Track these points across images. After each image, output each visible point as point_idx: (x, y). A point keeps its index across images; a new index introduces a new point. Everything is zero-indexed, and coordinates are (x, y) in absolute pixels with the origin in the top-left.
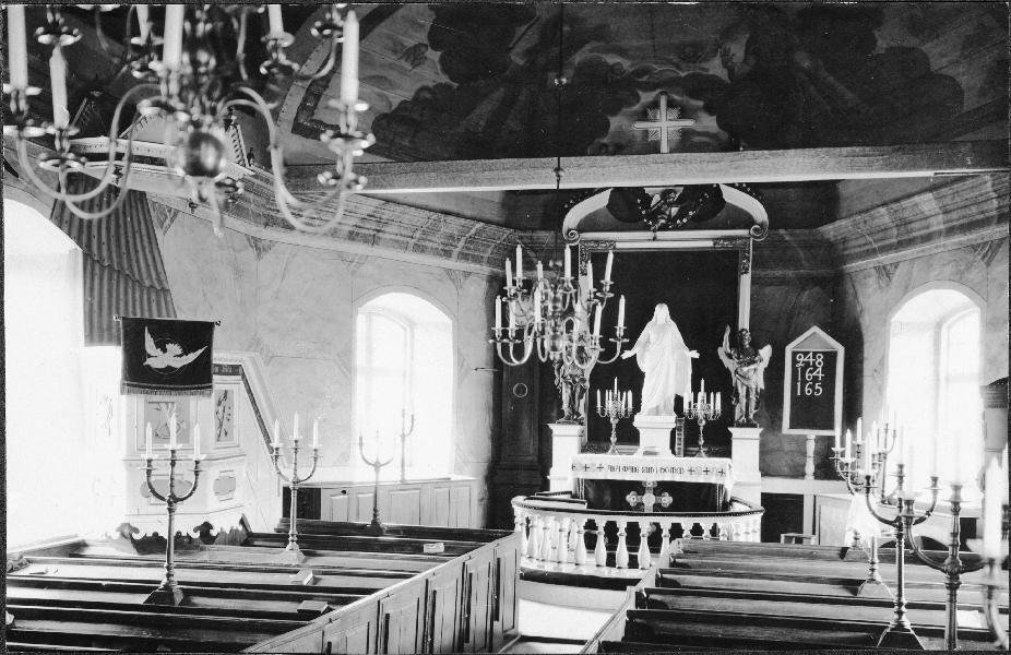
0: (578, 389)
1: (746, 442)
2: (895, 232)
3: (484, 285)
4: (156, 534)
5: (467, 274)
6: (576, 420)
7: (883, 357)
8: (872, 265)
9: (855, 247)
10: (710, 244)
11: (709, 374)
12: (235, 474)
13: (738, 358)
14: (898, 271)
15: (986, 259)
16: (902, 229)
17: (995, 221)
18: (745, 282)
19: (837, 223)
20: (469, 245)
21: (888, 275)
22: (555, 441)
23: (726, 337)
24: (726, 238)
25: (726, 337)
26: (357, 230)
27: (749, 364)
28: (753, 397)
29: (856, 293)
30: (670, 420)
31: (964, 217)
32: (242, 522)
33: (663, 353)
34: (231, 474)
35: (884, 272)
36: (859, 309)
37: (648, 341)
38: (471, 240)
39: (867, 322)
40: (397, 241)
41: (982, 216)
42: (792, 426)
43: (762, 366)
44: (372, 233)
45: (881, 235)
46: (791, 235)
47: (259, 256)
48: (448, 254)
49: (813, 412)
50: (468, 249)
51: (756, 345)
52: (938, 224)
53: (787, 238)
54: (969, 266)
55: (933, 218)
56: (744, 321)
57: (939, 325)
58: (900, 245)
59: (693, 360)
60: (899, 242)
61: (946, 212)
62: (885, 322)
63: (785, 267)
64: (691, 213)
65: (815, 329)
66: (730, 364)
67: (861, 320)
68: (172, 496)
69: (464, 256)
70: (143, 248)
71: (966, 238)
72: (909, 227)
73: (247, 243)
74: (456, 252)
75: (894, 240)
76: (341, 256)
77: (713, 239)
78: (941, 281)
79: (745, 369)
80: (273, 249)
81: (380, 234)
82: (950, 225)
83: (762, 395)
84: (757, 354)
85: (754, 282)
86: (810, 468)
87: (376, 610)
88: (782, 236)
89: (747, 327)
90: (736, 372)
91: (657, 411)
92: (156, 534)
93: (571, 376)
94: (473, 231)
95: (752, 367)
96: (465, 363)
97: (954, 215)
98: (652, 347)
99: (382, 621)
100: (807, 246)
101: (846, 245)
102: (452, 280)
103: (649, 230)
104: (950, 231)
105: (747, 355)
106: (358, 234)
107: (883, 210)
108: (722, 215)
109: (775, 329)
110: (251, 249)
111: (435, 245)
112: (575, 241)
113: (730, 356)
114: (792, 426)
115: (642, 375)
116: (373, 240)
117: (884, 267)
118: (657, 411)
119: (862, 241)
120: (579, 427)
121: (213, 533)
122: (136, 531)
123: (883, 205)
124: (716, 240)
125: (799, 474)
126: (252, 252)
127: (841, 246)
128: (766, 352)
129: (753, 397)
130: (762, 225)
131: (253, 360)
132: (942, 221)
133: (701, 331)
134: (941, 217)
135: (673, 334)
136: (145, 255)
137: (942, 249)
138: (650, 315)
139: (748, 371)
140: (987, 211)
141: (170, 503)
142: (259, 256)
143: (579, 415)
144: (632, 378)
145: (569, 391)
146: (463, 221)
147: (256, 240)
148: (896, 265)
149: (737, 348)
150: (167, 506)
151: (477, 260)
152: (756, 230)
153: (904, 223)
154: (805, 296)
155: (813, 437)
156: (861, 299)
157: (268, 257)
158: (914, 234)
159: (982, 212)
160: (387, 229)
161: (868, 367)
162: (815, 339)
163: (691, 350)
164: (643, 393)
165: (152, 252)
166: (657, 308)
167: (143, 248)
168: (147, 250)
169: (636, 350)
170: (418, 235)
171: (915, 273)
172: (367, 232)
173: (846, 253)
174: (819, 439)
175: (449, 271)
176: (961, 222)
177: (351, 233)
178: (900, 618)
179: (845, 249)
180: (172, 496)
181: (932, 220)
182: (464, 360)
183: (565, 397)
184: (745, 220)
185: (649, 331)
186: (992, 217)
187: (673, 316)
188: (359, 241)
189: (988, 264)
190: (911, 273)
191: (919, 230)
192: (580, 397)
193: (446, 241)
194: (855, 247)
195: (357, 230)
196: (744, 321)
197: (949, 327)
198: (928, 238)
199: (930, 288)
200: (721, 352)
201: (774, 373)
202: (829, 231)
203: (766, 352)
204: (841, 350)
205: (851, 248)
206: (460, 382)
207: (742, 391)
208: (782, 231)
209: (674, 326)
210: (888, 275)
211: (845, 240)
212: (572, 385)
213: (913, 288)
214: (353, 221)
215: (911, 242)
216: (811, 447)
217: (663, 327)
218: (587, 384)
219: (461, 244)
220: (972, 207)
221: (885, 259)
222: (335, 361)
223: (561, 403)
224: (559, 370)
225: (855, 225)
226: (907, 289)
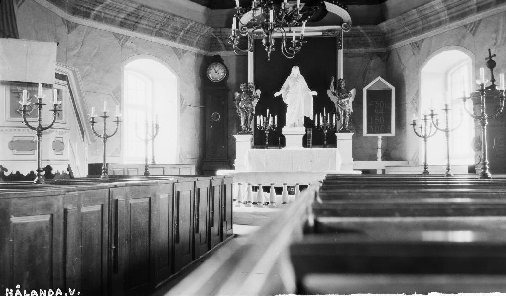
0: (250, 115)
1: (345, 140)
2: (421, 22)
3: (194, 57)
4: (18, 172)
5: (185, 51)
6: (249, 132)
7: (418, 91)
8: (408, 43)
9: (399, 34)
10: (320, 33)
11: (321, 104)
12: (64, 140)
13: (339, 95)
14: (423, 44)
15: (473, 32)
16: (425, 21)
17: (476, 11)
18: (341, 54)
19: (388, 21)
20: (186, 35)
21: (418, 47)
22: (237, 144)
23: (332, 84)
24: (329, 31)
25: (332, 84)
26: (125, 21)
27: (345, 98)
28: (347, 116)
29: (400, 59)
30: (303, 130)
31: (459, 11)
32: (68, 169)
33: (297, 94)
34: (61, 140)
35: (417, 46)
36: (402, 67)
37: (288, 87)
38: (188, 31)
39: (408, 74)
40: (146, 29)
41: (468, 9)
42: (368, 132)
43: (351, 100)
44: (133, 23)
45: (413, 25)
46: (363, 29)
47: (69, 32)
48: (174, 39)
49: (379, 123)
50: (185, 37)
51: (348, 89)
52: (445, 16)
53: (362, 31)
54: (464, 37)
55: (442, 13)
56: (341, 75)
57: (446, 74)
58: (423, 31)
59: (314, 96)
60: (423, 28)
61: (448, 9)
62: (417, 72)
63: (360, 47)
64: (309, 17)
65: (379, 78)
66: (334, 99)
67: (404, 73)
68: (40, 126)
69: (183, 41)
70: (7, 13)
71: (461, 21)
72: (428, 19)
73: (62, 23)
74: (178, 39)
75: (420, 28)
76: (116, 35)
77: (322, 31)
78: (449, 46)
79: (343, 100)
80: (77, 28)
81: (137, 24)
82: (451, 16)
83: (352, 115)
84: (349, 92)
85: (345, 55)
86: (379, 154)
87: (172, 188)
88: (359, 30)
89: (342, 78)
90: (338, 103)
91: (294, 125)
92: (18, 172)
93: (245, 107)
94: (188, 27)
95: (347, 99)
96: (184, 102)
97: (453, 10)
98: (290, 90)
99: (176, 195)
100: (371, 34)
101: (393, 34)
102: (177, 54)
103: (287, 26)
104: (452, 19)
105: (342, 93)
106: (125, 23)
107: (414, 11)
108: (326, 18)
109: (356, 80)
110: (64, 26)
111: (167, 33)
112: (246, 32)
113: (334, 94)
114: (368, 132)
115: (285, 106)
116: (133, 28)
117: (416, 43)
118: (294, 125)
119: (402, 30)
120: (251, 135)
121: (53, 172)
122: (7, 170)
123: (414, 9)
124: (323, 31)
125: (373, 158)
126: (64, 29)
127: (391, 34)
128: (353, 92)
129: (347, 116)
130: (348, 23)
131: (74, 73)
132: (446, 14)
133: (318, 80)
134: (446, 12)
135: (302, 83)
136: (7, 16)
137: (448, 29)
138: (288, 73)
139: (345, 101)
140: (471, 6)
141: (38, 131)
142: (69, 32)
143: (250, 129)
144: (280, 109)
145: (245, 116)
146: (183, 20)
147: (68, 22)
148: (423, 41)
149: (338, 89)
150: (36, 133)
151: (190, 44)
152: (345, 26)
153: (426, 17)
154: (372, 63)
155: (381, 137)
156: (403, 62)
157: (74, 32)
158: (432, 23)
159: (468, 7)
160: (142, 22)
161: (409, 99)
162: (378, 82)
163: (312, 90)
164: (287, 116)
165: (11, 15)
166: (293, 68)
167: (7, 13)
168: (9, 14)
169: (282, 92)
170: (158, 26)
171: (433, 44)
172: (130, 22)
173: (393, 38)
174: (384, 139)
175: (175, 49)
176: (457, 13)
177: (121, 22)
178: (485, 171)
179: (392, 36)
180: (40, 126)
181: (442, 14)
182: (184, 100)
183: (242, 120)
184: (339, 21)
185: (289, 81)
186: (474, 9)
187: (302, 73)
188: (126, 27)
189: (474, 34)
190: (431, 44)
191: (435, 20)
192: (251, 120)
193: (173, 31)
194: (399, 34)
195: (125, 21)
196: (341, 75)
197: (451, 75)
198: (440, 24)
199: (443, 50)
200: (329, 92)
201: (357, 103)
202: (384, 26)
203: (353, 92)
204: (393, 89)
205: (396, 35)
206: (182, 111)
207: (341, 113)
208: (359, 27)
209: (302, 78)
210: (418, 47)
211: (392, 30)
212: (246, 113)
213: (433, 52)
214: (123, 16)
215: (430, 28)
216: (380, 143)
217: (296, 79)
218: (254, 113)
219: (182, 33)
220: (462, 5)
221: (415, 39)
222: (111, 95)
223: (240, 123)
224: (238, 104)
225: (399, 21)
226: (429, 54)
